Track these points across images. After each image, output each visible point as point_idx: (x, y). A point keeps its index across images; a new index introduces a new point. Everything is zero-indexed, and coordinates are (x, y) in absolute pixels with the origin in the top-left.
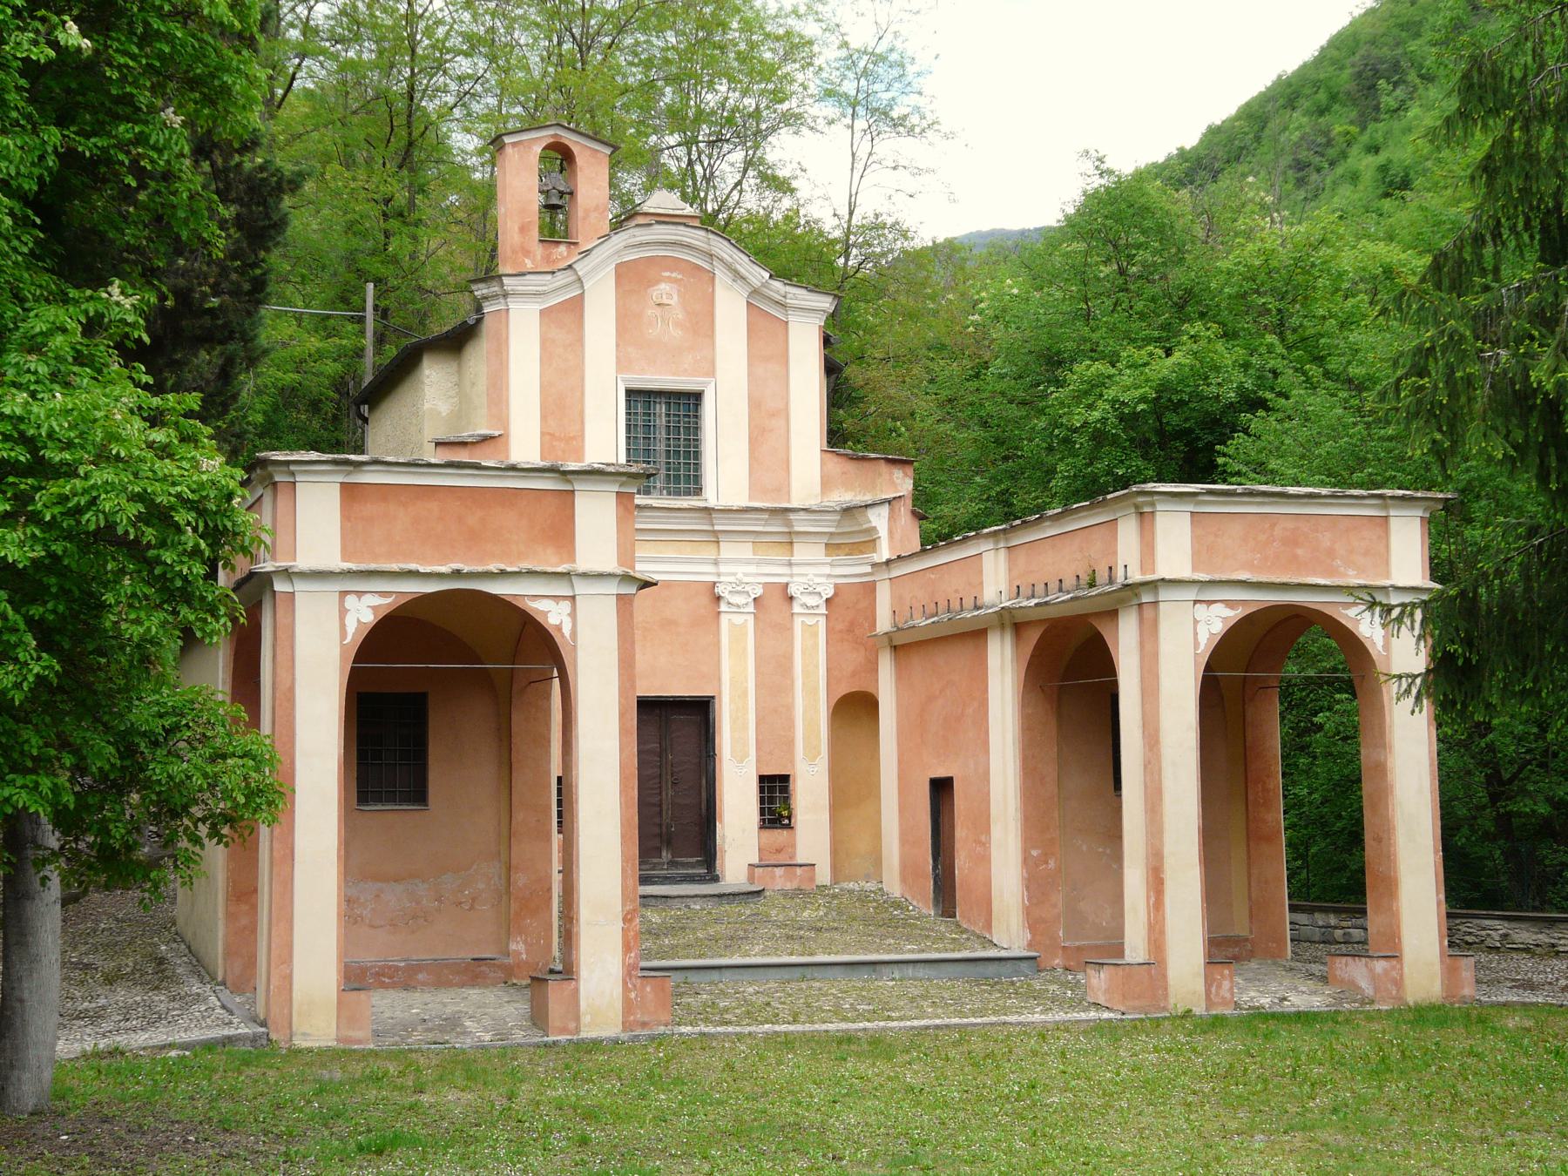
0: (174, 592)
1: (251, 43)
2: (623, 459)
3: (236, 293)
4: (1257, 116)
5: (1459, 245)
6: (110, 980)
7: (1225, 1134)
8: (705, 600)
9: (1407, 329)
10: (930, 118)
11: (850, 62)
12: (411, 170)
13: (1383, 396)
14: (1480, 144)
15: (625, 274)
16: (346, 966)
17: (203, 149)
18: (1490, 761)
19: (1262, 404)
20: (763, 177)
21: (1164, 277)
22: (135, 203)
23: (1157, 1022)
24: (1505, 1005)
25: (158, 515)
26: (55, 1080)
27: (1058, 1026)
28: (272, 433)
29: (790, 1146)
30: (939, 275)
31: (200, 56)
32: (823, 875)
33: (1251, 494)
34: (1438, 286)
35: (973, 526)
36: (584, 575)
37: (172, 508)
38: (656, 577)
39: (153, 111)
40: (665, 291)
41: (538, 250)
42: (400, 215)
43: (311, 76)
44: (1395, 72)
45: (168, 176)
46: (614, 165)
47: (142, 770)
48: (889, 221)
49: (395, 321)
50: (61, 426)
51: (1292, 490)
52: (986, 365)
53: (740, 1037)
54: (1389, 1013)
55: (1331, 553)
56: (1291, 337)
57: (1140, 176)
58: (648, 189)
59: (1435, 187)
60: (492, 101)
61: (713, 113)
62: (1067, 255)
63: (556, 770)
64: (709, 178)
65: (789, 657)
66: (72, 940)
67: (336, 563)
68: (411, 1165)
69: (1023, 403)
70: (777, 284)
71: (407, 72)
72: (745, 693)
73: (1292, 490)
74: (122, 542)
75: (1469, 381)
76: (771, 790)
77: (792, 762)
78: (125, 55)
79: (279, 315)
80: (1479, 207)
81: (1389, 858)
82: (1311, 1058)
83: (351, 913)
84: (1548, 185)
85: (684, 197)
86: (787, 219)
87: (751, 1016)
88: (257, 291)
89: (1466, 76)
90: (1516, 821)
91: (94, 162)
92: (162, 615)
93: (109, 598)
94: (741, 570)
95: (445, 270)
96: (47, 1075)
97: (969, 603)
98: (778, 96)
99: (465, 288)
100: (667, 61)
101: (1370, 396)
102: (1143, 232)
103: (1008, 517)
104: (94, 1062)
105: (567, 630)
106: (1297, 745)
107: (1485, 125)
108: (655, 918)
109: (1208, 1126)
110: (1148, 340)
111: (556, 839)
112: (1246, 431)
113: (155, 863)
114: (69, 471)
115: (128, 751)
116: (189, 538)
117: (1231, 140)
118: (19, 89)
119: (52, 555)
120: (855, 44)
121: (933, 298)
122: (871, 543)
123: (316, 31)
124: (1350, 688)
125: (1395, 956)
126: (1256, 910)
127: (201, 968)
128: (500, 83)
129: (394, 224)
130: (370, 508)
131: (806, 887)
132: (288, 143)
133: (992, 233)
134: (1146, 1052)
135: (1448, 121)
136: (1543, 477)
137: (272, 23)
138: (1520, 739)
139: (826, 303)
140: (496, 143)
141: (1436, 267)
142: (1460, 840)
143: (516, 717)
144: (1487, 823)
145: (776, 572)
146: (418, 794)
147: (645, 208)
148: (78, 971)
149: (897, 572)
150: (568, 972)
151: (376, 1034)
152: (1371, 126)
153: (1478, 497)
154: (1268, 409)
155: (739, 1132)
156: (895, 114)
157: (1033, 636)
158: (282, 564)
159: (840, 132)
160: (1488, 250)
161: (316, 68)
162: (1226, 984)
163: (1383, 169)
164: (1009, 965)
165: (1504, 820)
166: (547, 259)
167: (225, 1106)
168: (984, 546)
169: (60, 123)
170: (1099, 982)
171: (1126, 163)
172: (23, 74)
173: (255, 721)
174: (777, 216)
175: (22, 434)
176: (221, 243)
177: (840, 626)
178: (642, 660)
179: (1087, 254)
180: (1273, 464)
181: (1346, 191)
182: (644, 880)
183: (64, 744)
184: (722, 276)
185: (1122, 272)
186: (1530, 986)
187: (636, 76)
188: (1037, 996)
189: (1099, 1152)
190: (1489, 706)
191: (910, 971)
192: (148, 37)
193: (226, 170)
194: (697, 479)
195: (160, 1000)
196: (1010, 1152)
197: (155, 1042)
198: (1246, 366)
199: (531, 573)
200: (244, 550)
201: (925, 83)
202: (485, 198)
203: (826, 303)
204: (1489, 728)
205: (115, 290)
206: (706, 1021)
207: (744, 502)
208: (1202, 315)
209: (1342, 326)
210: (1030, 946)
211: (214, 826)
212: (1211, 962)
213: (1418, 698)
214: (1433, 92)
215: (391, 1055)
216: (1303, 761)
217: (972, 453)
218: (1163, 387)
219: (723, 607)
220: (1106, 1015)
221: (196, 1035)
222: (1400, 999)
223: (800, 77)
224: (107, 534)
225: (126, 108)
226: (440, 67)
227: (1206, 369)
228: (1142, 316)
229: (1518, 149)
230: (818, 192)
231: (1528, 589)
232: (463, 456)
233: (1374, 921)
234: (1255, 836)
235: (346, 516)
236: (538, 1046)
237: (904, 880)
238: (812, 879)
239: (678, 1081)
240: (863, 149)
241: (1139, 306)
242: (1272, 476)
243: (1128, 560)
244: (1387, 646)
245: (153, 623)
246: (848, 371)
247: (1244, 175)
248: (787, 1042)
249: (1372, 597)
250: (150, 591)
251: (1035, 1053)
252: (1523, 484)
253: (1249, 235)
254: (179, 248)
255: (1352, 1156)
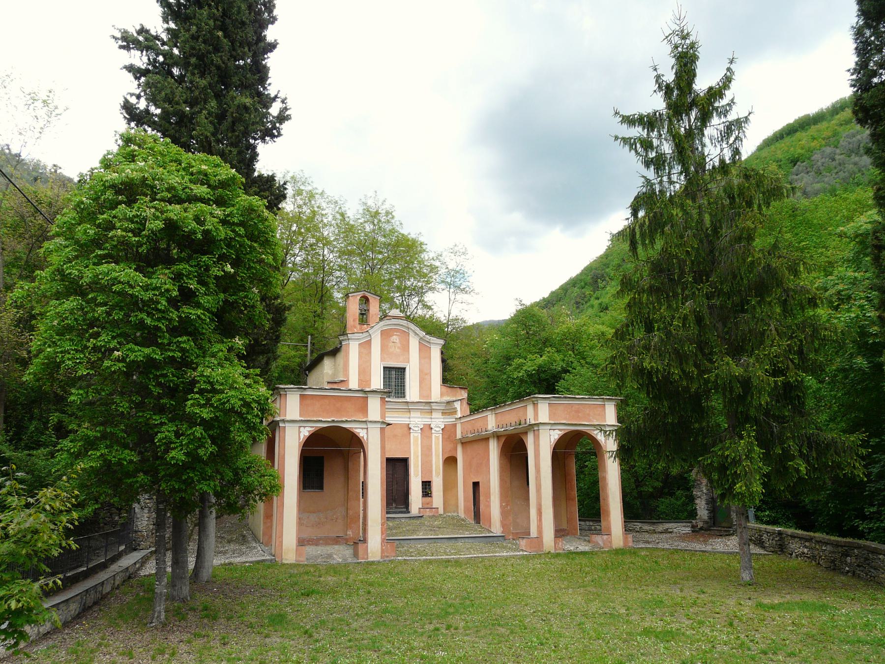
0: (251, 427)
1: (278, 269)
2: (382, 388)
3: (271, 339)
4: (565, 289)
5: (622, 326)
6: (229, 542)
7: (561, 589)
8: (406, 429)
9: (609, 350)
10: (472, 289)
11: (449, 273)
12: (323, 303)
13: (602, 370)
14: (627, 300)
15: (383, 333)
16: (299, 538)
17: (263, 299)
18: (635, 475)
19: (568, 371)
20: (424, 305)
21: (539, 334)
22: (244, 314)
23: (540, 555)
24: (641, 548)
25: (247, 404)
26: (213, 572)
27: (513, 557)
28: (280, 379)
29: (431, 594)
30: (475, 333)
31: (264, 273)
32: (441, 511)
33: (566, 398)
34: (617, 339)
35: (486, 407)
36: (371, 422)
37: (251, 402)
38: (391, 422)
39: (250, 288)
40: (395, 338)
41: (358, 326)
42: (319, 316)
43: (295, 276)
44: (603, 278)
45: (253, 307)
46: (381, 302)
47: (240, 480)
48: (460, 318)
49: (316, 346)
50: (220, 378)
51: (577, 396)
52: (489, 360)
53: (416, 560)
54: (608, 551)
55: (589, 415)
56: (576, 352)
57: (532, 306)
58: (390, 309)
59: (615, 310)
60: (346, 284)
61: (409, 287)
62: (511, 328)
63: (362, 480)
64: (408, 306)
65: (431, 446)
66: (218, 530)
67: (297, 417)
68: (317, 599)
69: (499, 371)
70: (427, 336)
71: (322, 276)
72: (418, 456)
73: (577, 396)
74: (236, 412)
75: (626, 366)
76: (426, 485)
77: (432, 477)
78: (243, 273)
79: (283, 345)
80: (627, 316)
81: (607, 505)
82: (586, 566)
83: (300, 522)
84: (646, 311)
85: (401, 311)
86: (430, 317)
87: (419, 554)
88: (277, 339)
89: (622, 280)
90: (643, 493)
91: (233, 303)
92: (247, 434)
93: (232, 429)
94: (417, 420)
95: (331, 332)
96: (210, 570)
97: (484, 430)
98: (428, 282)
99: (337, 337)
100: (396, 273)
101: (599, 370)
102: (534, 322)
103: (495, 404)
104: (225, 567)
105: (365, 438)
106: (580, 471)
107: (628, 294)
108: (391, 524)
109: (556, 587)
110: (536, 353)
111: (362, 500)
112: (564, 379)
113: (243, 507)
114: (221, 391)
115: (236, 474)
116: (256, 411)
117: (558, 295)
118: (213, 283)
119: (216, 416)
120: (450, 267)
121: (473, 340)
122: (455, 412)
123: (296, 264)
124: (595, 454)
125: (609, 534)
126: (569, 521)
127: (256, 539)
128: (348, 279)
129: (317, 318)
130: (308, 402)
131: (436, 515)
132: (287, 296)
133: (490, 321)
134: (537, 564)
135: (618, 292)
136: (648, 394)
137: (284, 264)
138: (644, 469)
139: (442, 342)
140: (347, 296)
141: (616, 333)
142: (627, 499)
143: (350, 464)
144: (635, 494)
145: (427, 421)
146: (321, 487)
147: (389, 314)
148: (220, 539)
149: (463, 420)
150: (365, 541)
151: (307, 559)
152: (597, 292)
153: (630, 399)
154: (570, 373)
155: (415, 590)
156: (461, 287)
157: (503, 440)
158: (282, 418)
159: (446, 292)
160: (630, 329)
161: (296, 275)
162: (560, 544)
163: (600, 304)
164: (496, 538)
165: (640, 493)
166: (361, 329)
167: (262, 580)
168: (488, 413)
169: (224, 292)
170: (523, 543)
171: (528, 301)
172: (214, 279)
173: (273, 465)
174: (427, 316)
175: (209, 381)
176: (267, 325)
177: (446, 437)
178: (387, 447)
179: (517, 328)
180: (572, 389)
181: (590, 310)
182: (388, 513)
183: (218, 472)
184: (411, 334)
185: (527, 333)
186: (648, 542)
187: (387, 277)
188: (505, 547)
189: (524, 595)
190: (634, 460)
191: (467, 540)
192: (250, 268)
193: (270, 304)
194: (404, 393)
195: (244, 548)
196: (496, 595)
197: (242, 561)
198: (563, 360)
199: (355, 421)
200: (271, 415)
201: (470, 279)
202: (343, 311)
203: (442, 342)
204: (635, 466)
205: (237, 339)
206: (406, 555)
207: (418, 400)
208: (551, 346)
209: (590, 349)
210: (502, 532)
211: (260, 497)
212: (556, 537)
213: (615, 458)
214: (613, 283)
215: (314, 566)
216: (582, 476)
217: (484, 385)
218: (540, 366)
219: (411, 431)
220: (525, 553)
221: (254, 559)
222: (611, 547)
223: (434, 277)
224: (232, 410)
225: (243, 288)
226: (331, 274)
227: (552, 361)
228: (534, 346)
229: (637, 300)
230: (440, 309)
231: (645, 425)
232: (335, 386)
233: (603, 523)
234: (568, 499)
235: (301, 404)
236: (355, 563)
237: (465, 513)
238: (438, 512)
239: (398, 574)
240: (452, 297)
241: (533, 343)
242: (572, 392)
243: (530, 418)
244: (605, 442)
245: (245, 436)
246: (448, 361)
247: (562, 306)
248: (430, 562)
249: (601, 428)
250: (243, 427)
251: (504, 565)
252: (642, 396)
253: (563, 323)
254: (255, 327)
255: (597, 595)
